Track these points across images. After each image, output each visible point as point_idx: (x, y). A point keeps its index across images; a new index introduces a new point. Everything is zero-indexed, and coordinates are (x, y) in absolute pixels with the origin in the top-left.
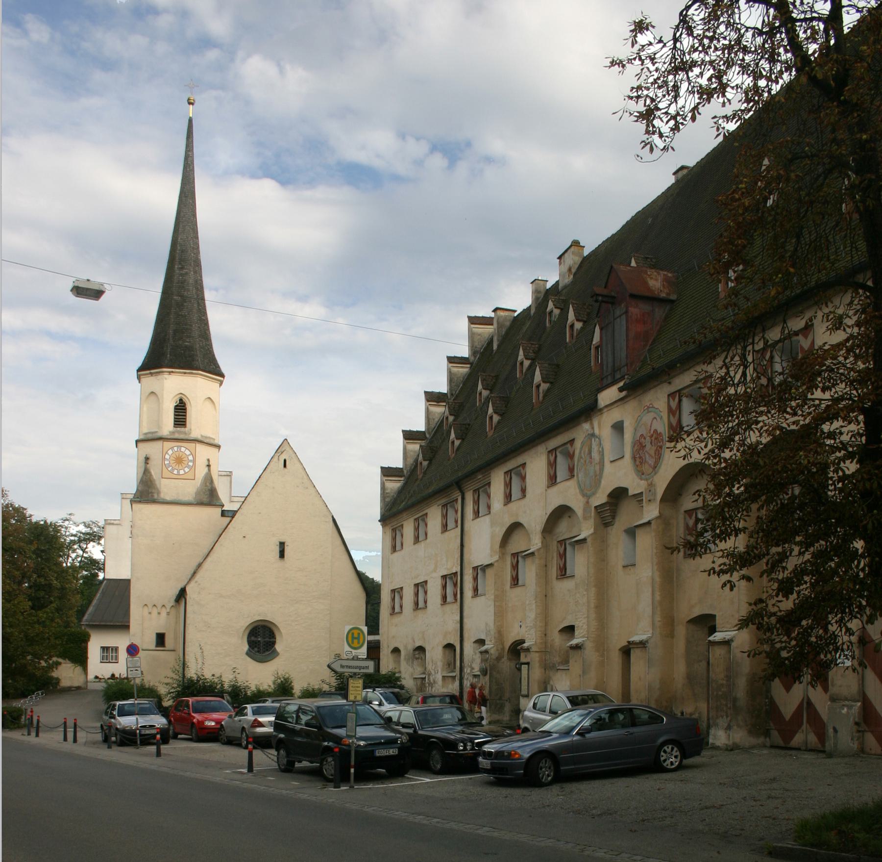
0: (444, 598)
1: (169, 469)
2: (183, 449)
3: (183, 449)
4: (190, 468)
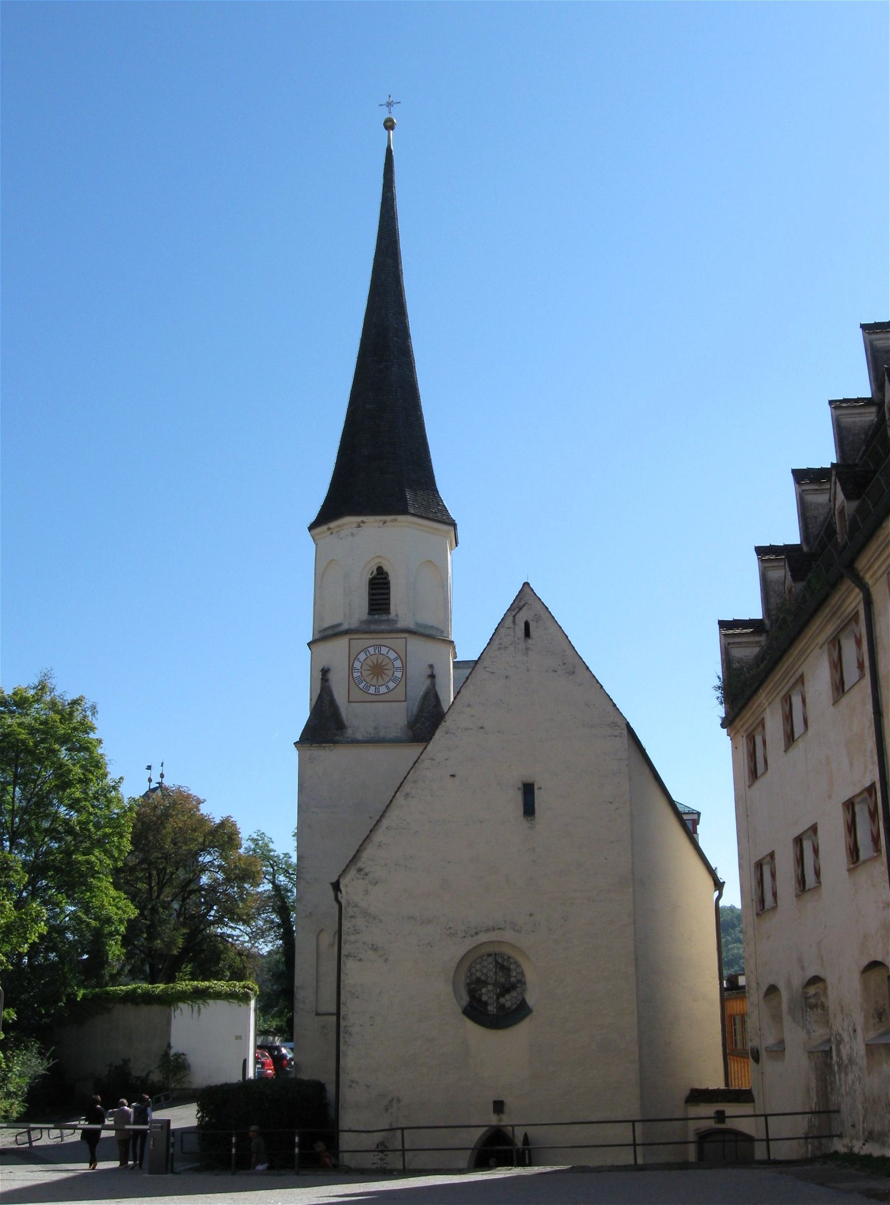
0: (854, 852)
1: (361, 686)
2: (384, 650)
3: (384, 650)
4: (397, 681)
